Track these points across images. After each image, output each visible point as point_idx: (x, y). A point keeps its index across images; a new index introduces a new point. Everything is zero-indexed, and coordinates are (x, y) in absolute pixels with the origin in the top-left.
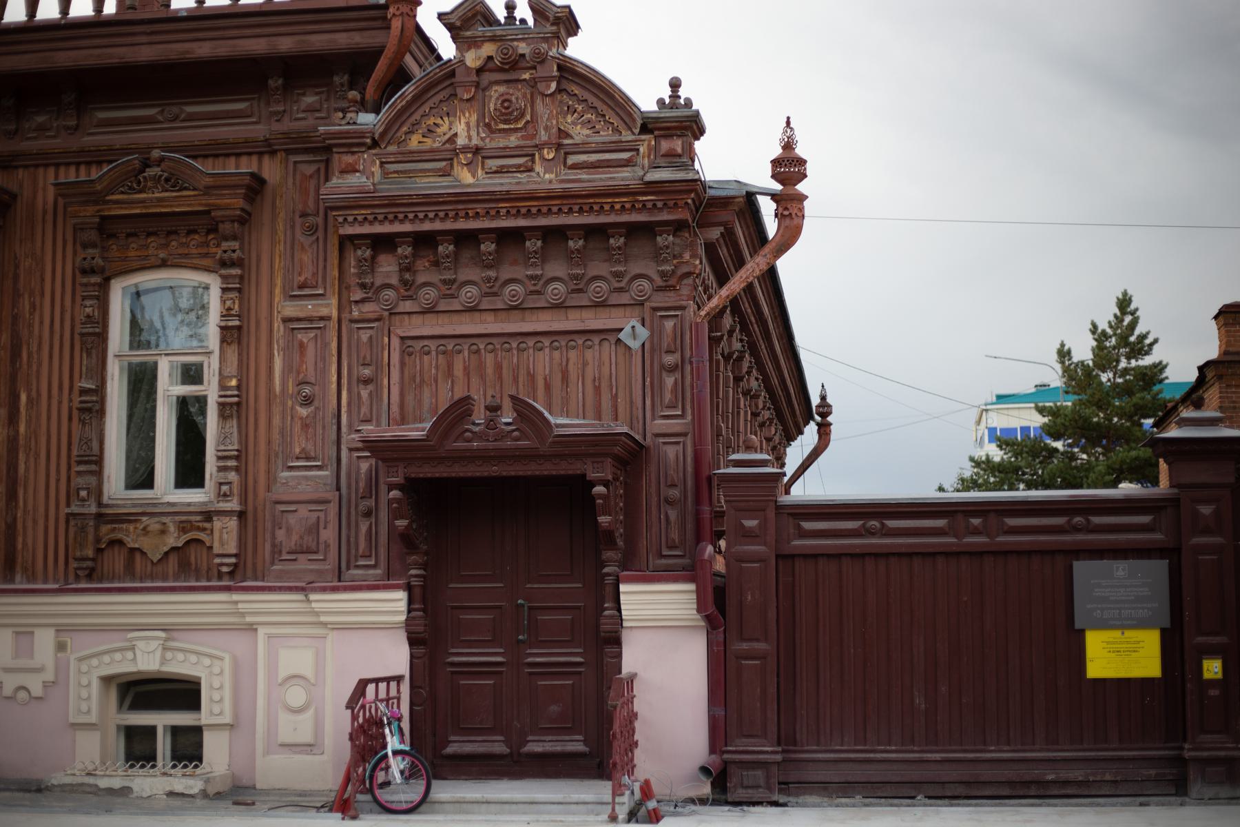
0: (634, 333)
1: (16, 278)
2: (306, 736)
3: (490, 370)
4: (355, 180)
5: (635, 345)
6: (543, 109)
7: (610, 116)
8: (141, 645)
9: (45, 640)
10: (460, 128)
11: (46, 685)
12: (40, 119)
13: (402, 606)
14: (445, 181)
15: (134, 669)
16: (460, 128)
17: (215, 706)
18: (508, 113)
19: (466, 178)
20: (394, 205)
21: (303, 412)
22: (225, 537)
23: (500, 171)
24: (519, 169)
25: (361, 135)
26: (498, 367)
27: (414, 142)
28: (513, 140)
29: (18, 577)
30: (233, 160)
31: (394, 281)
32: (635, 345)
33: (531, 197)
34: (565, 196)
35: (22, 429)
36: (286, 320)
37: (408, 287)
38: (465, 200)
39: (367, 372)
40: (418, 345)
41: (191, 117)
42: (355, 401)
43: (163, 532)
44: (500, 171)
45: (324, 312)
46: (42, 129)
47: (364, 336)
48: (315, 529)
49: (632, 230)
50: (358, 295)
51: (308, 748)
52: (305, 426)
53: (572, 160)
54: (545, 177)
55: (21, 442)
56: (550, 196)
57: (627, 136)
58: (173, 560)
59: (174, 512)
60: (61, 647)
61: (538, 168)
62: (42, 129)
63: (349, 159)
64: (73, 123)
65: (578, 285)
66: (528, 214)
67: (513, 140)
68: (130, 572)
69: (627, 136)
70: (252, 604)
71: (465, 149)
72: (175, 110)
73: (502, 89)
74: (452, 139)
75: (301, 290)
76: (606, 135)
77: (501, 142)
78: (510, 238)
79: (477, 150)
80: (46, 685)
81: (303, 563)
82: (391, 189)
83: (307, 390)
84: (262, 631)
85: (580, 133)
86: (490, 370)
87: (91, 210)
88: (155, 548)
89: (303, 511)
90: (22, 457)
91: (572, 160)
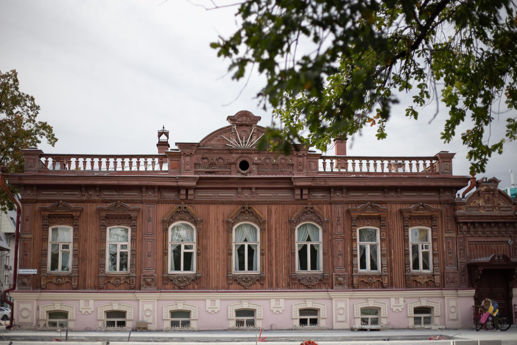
0: (511, 242)
1: (389, 227)
2: (455, 318)
3: (484, 248)
4: (461, 211)
5: (511, 244)
6: (495, 199)
7: (507, 201)
8: (56, 304)
9: (401, 300)
10: (480, 202)
11: (283, 310)
12: (392, 194)
13: (474, 293)
14: (478, 212)
15: (306, 307)
16: (480, 202)
17: (322, 314)
18: (488, 200)
19: (483, 212)
20: (470, 217)
21: (450, 255)
22: (437, 279)
23: (488, 211)
24: (491, 210)
25: (463, 202)
26: (486, 248)
27: (472, 204)
28: (490, 205)
29: (394, 287)
30: (384, 205)
31: (466, 230)
32: (511, 244)
33: (495, 216)
34: (501, 216)
35: (393, 257)
36: (446, 237)
37: (468, 231)
38: (482, 216)
39: (462, 248)
40: (471, 243)
41: (423, 196)
42: (460, 253)
43: (424, 278)
44: (488, 211)
45: (453, 236)
46: (150, 196)
47: (461, 241)
48: (454, 278)
49: (510, 223)
50: (459, 233)
51: (455, 320)
52: (451, 258)
53: (501, 209)
54: (496, 213)
55: (393, 260)
56: (498, 216)
57: (510, 205)
58: (425, 284)
59: (423, 275)
60: (404, 301)
61: (495, 210)
62: (392, 196)
63: (460, 207)
64: (98, 194)
65: (499, 232)
66: (494, 219)
67: (490, 205)
68: (417, 286)
69: (510, 205)
70: (139, 295)
71: (482, 206)
72: (61, 193)
73: (487, 195)
74: (479, 204)
75: (448, 231)
76: (506, 205)
77: (487, 205)
78: (489, 223)
79: (484, 207)
80: (283, 310)
81: (452, 285)
82: (468, 213)
83: (450, 251)
84: (446, 298)
85: (502, 204)
86: (484, 248)
87: (408, 214)
88: (423, 282)
89: (451, 275)
90: (393, 263)
91: (501, 209)
